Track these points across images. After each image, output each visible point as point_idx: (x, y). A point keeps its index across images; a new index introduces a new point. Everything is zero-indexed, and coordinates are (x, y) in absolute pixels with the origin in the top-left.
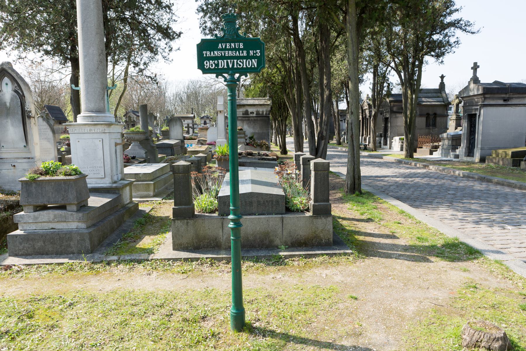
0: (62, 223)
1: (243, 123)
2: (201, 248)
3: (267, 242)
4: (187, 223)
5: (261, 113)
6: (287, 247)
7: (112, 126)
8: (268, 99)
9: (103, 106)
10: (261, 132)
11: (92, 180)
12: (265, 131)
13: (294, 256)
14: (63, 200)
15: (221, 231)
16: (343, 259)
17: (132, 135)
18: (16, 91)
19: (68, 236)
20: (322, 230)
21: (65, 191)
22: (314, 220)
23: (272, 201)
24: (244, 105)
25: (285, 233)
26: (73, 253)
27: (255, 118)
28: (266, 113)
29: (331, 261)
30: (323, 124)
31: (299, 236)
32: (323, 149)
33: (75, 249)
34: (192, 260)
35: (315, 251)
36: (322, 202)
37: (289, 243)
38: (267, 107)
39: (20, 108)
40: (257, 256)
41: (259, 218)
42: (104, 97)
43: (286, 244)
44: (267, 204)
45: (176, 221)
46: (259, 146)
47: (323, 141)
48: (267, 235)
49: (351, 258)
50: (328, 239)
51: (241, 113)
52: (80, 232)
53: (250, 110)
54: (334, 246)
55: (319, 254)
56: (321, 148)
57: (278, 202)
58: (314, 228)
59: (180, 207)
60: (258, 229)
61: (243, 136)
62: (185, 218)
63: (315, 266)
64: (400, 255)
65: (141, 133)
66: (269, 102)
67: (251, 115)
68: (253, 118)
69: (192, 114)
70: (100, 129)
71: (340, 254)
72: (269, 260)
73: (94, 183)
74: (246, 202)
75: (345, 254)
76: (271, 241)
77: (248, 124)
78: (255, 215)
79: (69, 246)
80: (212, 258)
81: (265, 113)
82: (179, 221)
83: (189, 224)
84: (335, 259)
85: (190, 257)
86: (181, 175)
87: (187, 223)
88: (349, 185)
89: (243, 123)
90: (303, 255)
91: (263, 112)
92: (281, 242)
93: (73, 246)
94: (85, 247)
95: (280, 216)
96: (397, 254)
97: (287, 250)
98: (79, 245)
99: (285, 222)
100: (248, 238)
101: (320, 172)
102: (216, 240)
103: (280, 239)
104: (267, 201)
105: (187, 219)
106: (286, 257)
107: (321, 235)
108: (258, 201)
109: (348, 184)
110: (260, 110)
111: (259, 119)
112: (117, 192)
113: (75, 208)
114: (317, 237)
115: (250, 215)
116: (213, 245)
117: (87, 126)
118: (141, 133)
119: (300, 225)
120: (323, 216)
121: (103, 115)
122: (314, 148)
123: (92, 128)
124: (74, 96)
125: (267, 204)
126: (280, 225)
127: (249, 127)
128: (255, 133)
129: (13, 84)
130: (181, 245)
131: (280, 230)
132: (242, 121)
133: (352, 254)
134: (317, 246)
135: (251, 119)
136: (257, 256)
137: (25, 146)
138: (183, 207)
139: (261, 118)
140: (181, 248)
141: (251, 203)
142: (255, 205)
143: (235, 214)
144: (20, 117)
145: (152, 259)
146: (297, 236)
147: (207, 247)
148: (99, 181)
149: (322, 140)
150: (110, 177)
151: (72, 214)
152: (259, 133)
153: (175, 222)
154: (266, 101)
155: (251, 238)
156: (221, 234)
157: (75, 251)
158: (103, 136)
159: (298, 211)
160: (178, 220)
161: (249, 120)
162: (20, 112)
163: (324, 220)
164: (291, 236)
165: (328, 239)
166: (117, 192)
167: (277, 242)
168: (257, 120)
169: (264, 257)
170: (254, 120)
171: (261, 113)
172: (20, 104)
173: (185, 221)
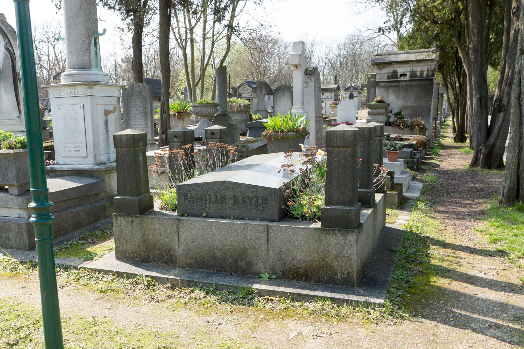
0: (5, 209)
1: (387, 91)
2: (151, 262)
3: (243, 264)
4: (132, 222)
5: (418, 74)
6: (274, 277)
7: (97, 87)
8: (433, 52)
9: (88, 60)
10: (416, 104)
11: (74, 159)
12: (423, 103)
13: (275, 293)
14: (3, 179)
15: (176, 238)
16: (359, 313)
17: (200, 109)
18: (7, 49)
19: (6, 226)
20: (337, 255)
21: (6, 169)
22: (323, 237)
23: (257, 198)
24: (390, 63)
25: (271, 254)
26: (13, 248)
27: (408, 83)
28: (427, 75)
29: (333, 312)
30: (503, 85)
31: (296, 262)
32: (500, 128)
33: (13, 243)
34: (129, 276)
35: (315, 290)
36: (340, 205)
37: (279, 271)
38: (429, 63)
39: (11, 69)
40: (216, 285)
41: (230, 224)
42: (89, 47)
43: (272, 271)
44: (248, 201)
45: (119, 218)
46: (408, 126)
47: (502, 115)
48: (242, 252)
49: (375, 314)
50: (348, 274)
51: (386, 76)
52: (19, 222)
53: (400, 70)
54: (358, 286)
55: (317, 297)
56: (497, 128)
57: (266, 200)
58: (322, 249)
59: (124, 197)
60: (229, 242)
61: (383, 111)
62: (129, 215)
63: (299, 316)
64: (491, 326)
65: (211, 106)
66: (434, 56)
67: (402, 78)
68: (404, 84)
69: (335, 84)
70: (80, 90)
71: (357, 303)
72: (233, 293)
73: (76, 163)
74: (216, 196)
75: (367, 305)
76: (250, 265)
77: (395, 92)
78: (230, 218)
79: (8, 238)
80: (153, 278)
81: (425, 74)
82: (122, 219)
83: (135, 223)
84: (344, 310)
85: (128, 271)
86: (124, 149)
87: (132, 222)
88: (506, 190)
89: (387, 91)
90: (291, 294)
91: (422, 72)
92: (265, 268)
93: (12, 238)
94: (23, 242)
95: (266, 223)
96: (486, 322)
97: (271, 281)
98: (18, 239)
99: (271, 234)
100: (214, 254)
101: (337, 150)
102: (169, 251)
103: (264, 262)
104: (248, 197)
105: (132, 217)
106: (260, 293)
107: (335, 264)
108: (235, 197)
109: (504, 188)
110: (418, 69)
111: (414, 83)
112: (100, 176)
113: (15, 191)
114: (327, 266)
115: (222, 217)
116: (165, 258)
117: (66, 88)
118: (211, 106)
119: (297, 240)
120: (340, 231)
121: (86, 72)
122: (483, 126)
123: (72, 89)
124: (135, 59)
125: (248, 201)
126: (265, 239)
127: (397, 97)
128: (405, 108)
129: (4, 40)
130: (125, 252)
131: (264, 247)
132: (387, 88)
133: (380, 305)
134: (326, 282)
135: (400, 84)
136: (216, 285)
137: (18, 117)
138: (128, 197)
139: (418, 82)
140: (126, 258)
141: (223, 198)
142: (230, 202)
143: (36, 201)
144: (11, 81)
145: (82, 268)
146: (293, 260)
147: (159, 261)
148: (81, 161)
149: (500, 111)
150: (93, 156)
151: (12, 198)
152: (412, 107)
153: (117, 219)
154: (431, 54)
155: (219, 255)
156: (176, 243)
157: (14, 246)
158: (84, 100)
159: (304, 218)
160: (121, 216)
161: (397, 86)
162: (11, 75)
163: (340, 237)
164: (281, 260)
165: (348, 274)
166: (100, 176)
167: (259, 266)
168: (412, 86)
169: (228, 287)
170: (407, 86)
171: (418, 74)
172: (11, 65)
173: (130, 218)
